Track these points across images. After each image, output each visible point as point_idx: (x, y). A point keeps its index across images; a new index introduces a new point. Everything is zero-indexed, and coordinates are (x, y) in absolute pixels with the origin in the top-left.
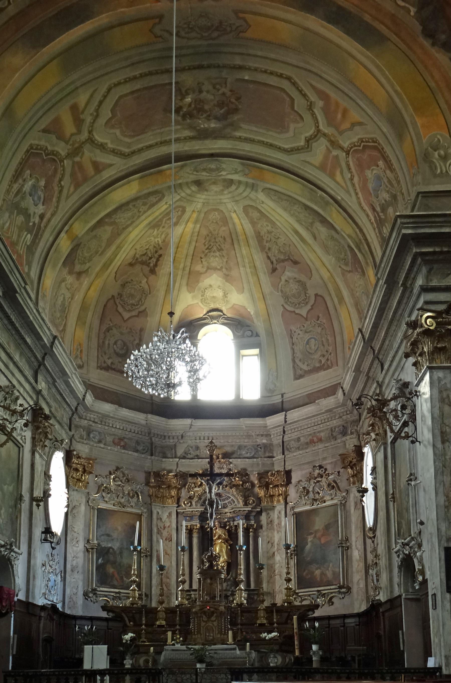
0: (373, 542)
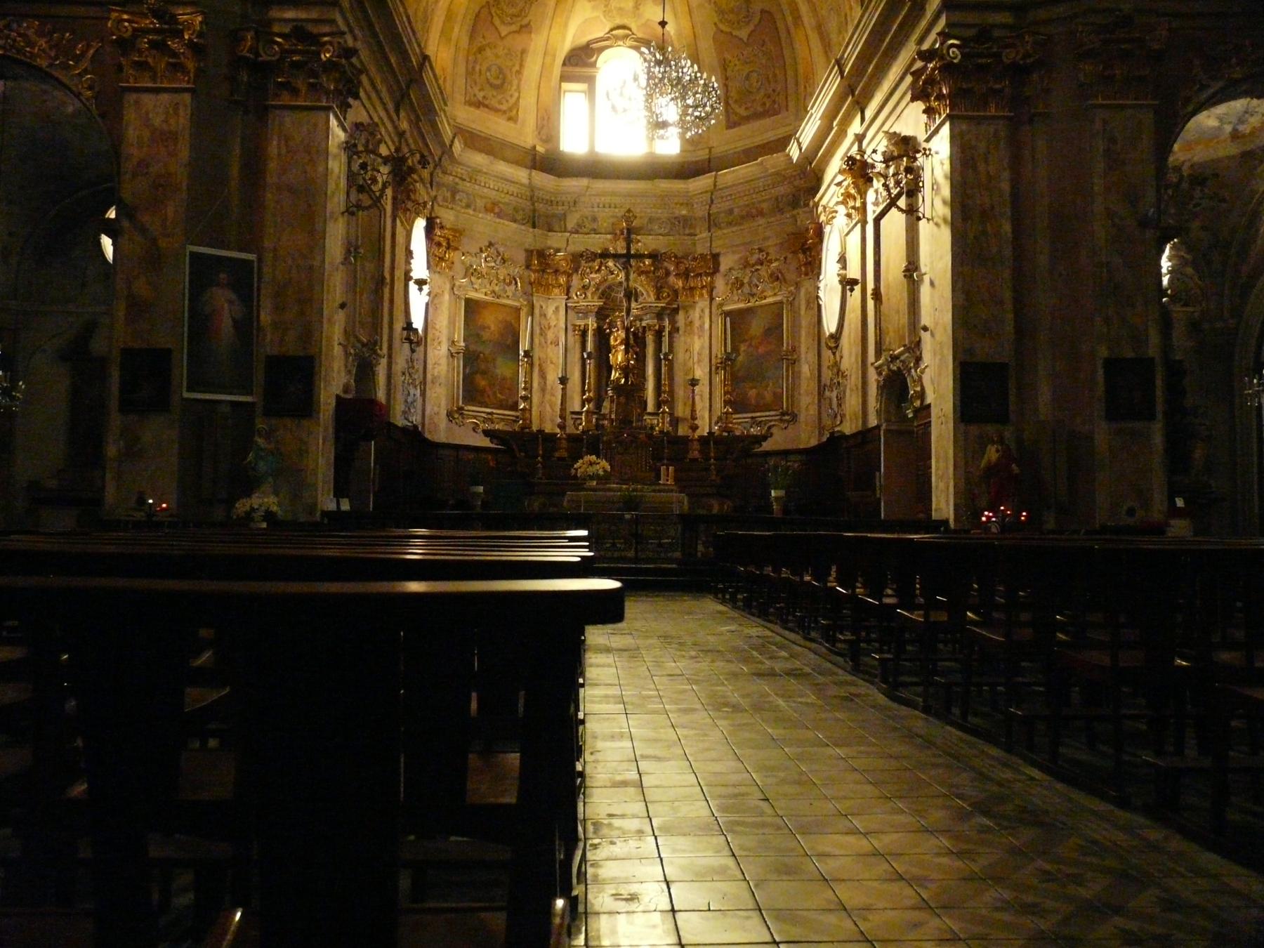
0: (834, 354)
